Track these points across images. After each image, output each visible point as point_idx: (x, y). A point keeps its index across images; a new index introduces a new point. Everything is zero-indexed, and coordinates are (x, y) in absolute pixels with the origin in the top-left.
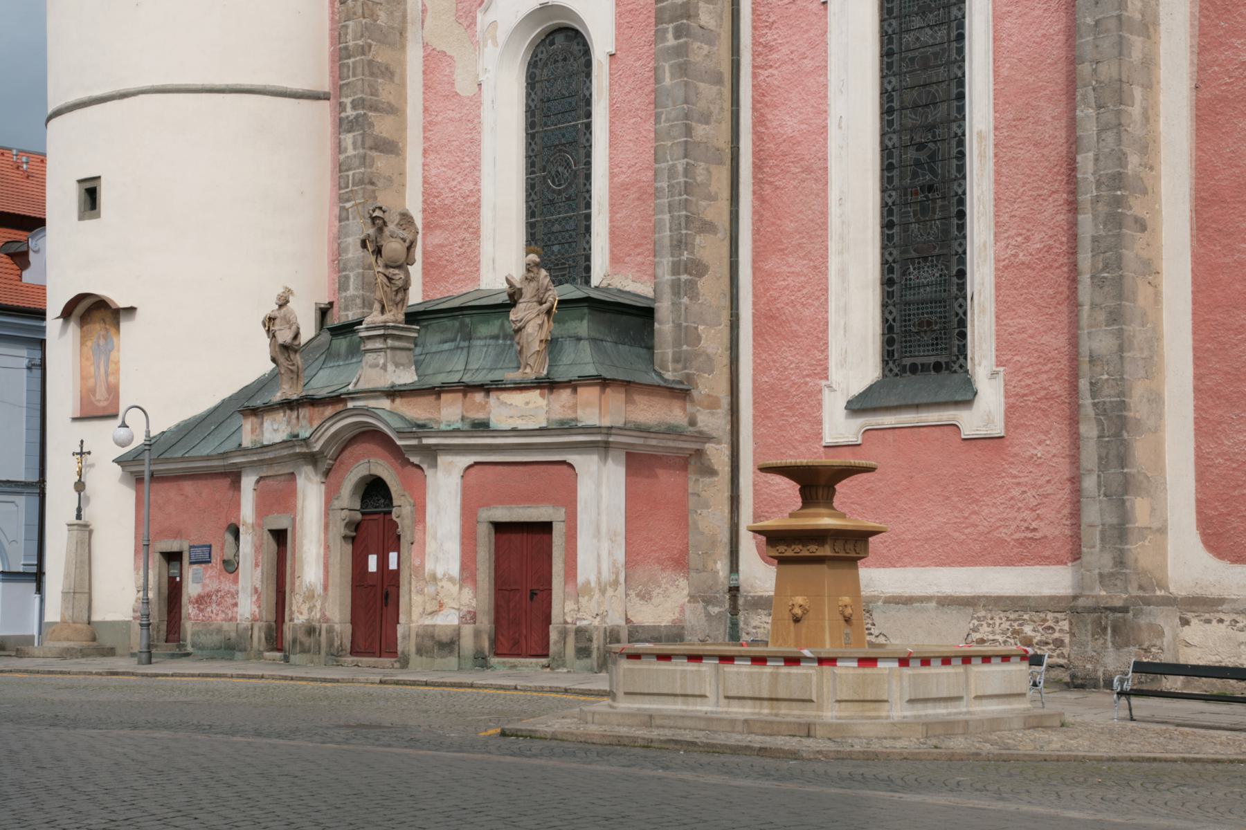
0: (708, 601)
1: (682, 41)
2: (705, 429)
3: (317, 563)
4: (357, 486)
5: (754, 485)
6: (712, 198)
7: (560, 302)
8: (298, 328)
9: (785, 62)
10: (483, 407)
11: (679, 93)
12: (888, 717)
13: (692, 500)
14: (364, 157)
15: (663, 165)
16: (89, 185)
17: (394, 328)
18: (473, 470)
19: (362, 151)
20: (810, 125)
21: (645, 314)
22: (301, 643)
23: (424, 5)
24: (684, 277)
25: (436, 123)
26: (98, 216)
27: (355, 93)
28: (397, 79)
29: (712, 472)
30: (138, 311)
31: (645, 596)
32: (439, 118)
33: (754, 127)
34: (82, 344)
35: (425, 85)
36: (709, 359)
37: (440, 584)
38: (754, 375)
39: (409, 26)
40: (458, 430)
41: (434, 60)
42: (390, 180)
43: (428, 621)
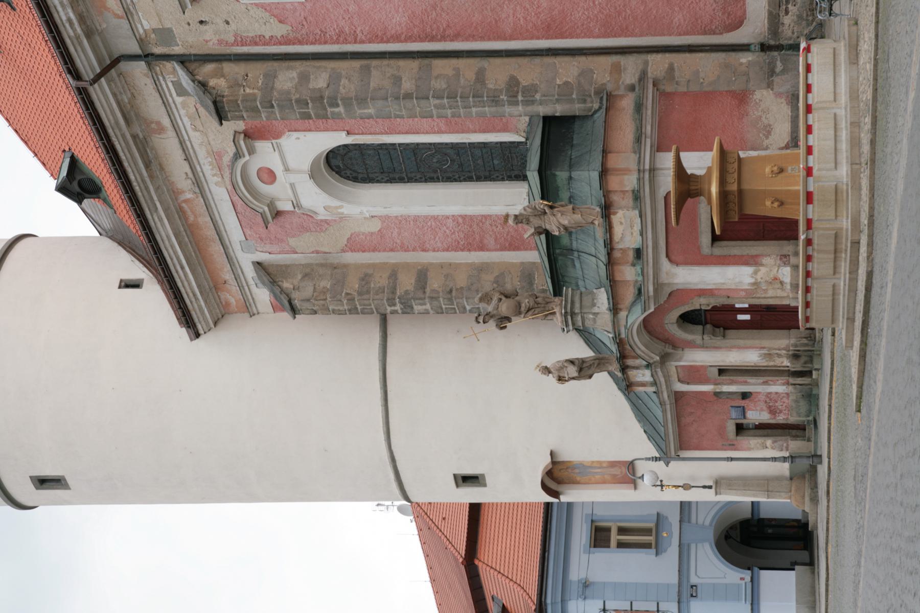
0: (772, 72)
1: (340, 102)
2: (637, 76)
3: (745, 352)
4: (686, 331)
5: (680, 35)
6: (458, 73)
7: (543, 198)
8: (567, 361)
9: (352, 23)
10: (624, 251)
11: (380, 103)
12: (847, 185)
13: (694, 88)
14: (431, 298)
15: (434, 112)
16: (460, 481)
17: (566, 308)
18: (673, 258)
19: (427, 300)
20: (399, 6)
21: (549, 121)
22: (805, 363)
23: (313, 252)
24: (520, 98)
25: (402, 243)
26: (483, 476)
27: (383, 304)
28: (370, 271)
29: (671, 68)
30: (552, 448)
31: (768, 131)
32: (398, 241)
33: (401, 42)
34: (578, 483)
35: (373, 251)
36: (582, 73)
37: (759, 280)
38: (594, 37)
39: (328, 261)
40: (642, 270)
41: (353, 245)
42: (447, 276)
43: (788, 287)
